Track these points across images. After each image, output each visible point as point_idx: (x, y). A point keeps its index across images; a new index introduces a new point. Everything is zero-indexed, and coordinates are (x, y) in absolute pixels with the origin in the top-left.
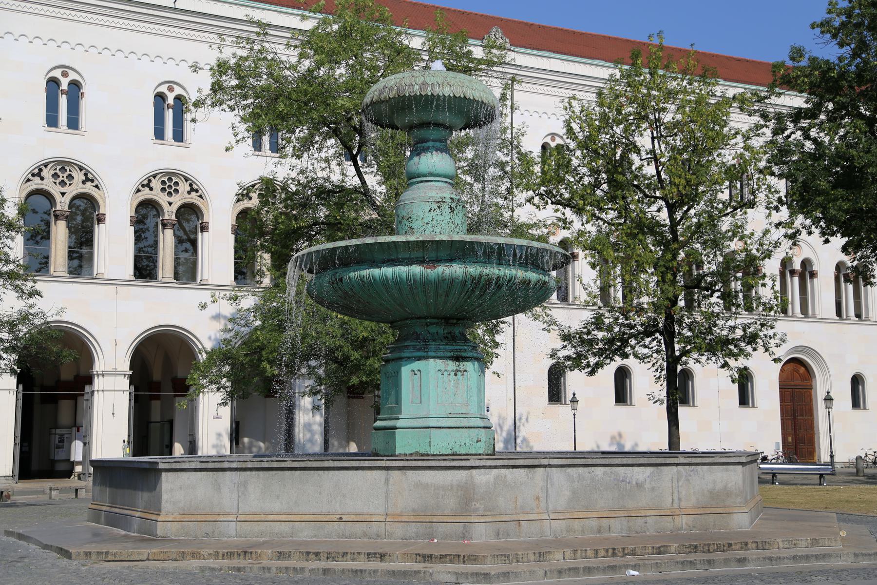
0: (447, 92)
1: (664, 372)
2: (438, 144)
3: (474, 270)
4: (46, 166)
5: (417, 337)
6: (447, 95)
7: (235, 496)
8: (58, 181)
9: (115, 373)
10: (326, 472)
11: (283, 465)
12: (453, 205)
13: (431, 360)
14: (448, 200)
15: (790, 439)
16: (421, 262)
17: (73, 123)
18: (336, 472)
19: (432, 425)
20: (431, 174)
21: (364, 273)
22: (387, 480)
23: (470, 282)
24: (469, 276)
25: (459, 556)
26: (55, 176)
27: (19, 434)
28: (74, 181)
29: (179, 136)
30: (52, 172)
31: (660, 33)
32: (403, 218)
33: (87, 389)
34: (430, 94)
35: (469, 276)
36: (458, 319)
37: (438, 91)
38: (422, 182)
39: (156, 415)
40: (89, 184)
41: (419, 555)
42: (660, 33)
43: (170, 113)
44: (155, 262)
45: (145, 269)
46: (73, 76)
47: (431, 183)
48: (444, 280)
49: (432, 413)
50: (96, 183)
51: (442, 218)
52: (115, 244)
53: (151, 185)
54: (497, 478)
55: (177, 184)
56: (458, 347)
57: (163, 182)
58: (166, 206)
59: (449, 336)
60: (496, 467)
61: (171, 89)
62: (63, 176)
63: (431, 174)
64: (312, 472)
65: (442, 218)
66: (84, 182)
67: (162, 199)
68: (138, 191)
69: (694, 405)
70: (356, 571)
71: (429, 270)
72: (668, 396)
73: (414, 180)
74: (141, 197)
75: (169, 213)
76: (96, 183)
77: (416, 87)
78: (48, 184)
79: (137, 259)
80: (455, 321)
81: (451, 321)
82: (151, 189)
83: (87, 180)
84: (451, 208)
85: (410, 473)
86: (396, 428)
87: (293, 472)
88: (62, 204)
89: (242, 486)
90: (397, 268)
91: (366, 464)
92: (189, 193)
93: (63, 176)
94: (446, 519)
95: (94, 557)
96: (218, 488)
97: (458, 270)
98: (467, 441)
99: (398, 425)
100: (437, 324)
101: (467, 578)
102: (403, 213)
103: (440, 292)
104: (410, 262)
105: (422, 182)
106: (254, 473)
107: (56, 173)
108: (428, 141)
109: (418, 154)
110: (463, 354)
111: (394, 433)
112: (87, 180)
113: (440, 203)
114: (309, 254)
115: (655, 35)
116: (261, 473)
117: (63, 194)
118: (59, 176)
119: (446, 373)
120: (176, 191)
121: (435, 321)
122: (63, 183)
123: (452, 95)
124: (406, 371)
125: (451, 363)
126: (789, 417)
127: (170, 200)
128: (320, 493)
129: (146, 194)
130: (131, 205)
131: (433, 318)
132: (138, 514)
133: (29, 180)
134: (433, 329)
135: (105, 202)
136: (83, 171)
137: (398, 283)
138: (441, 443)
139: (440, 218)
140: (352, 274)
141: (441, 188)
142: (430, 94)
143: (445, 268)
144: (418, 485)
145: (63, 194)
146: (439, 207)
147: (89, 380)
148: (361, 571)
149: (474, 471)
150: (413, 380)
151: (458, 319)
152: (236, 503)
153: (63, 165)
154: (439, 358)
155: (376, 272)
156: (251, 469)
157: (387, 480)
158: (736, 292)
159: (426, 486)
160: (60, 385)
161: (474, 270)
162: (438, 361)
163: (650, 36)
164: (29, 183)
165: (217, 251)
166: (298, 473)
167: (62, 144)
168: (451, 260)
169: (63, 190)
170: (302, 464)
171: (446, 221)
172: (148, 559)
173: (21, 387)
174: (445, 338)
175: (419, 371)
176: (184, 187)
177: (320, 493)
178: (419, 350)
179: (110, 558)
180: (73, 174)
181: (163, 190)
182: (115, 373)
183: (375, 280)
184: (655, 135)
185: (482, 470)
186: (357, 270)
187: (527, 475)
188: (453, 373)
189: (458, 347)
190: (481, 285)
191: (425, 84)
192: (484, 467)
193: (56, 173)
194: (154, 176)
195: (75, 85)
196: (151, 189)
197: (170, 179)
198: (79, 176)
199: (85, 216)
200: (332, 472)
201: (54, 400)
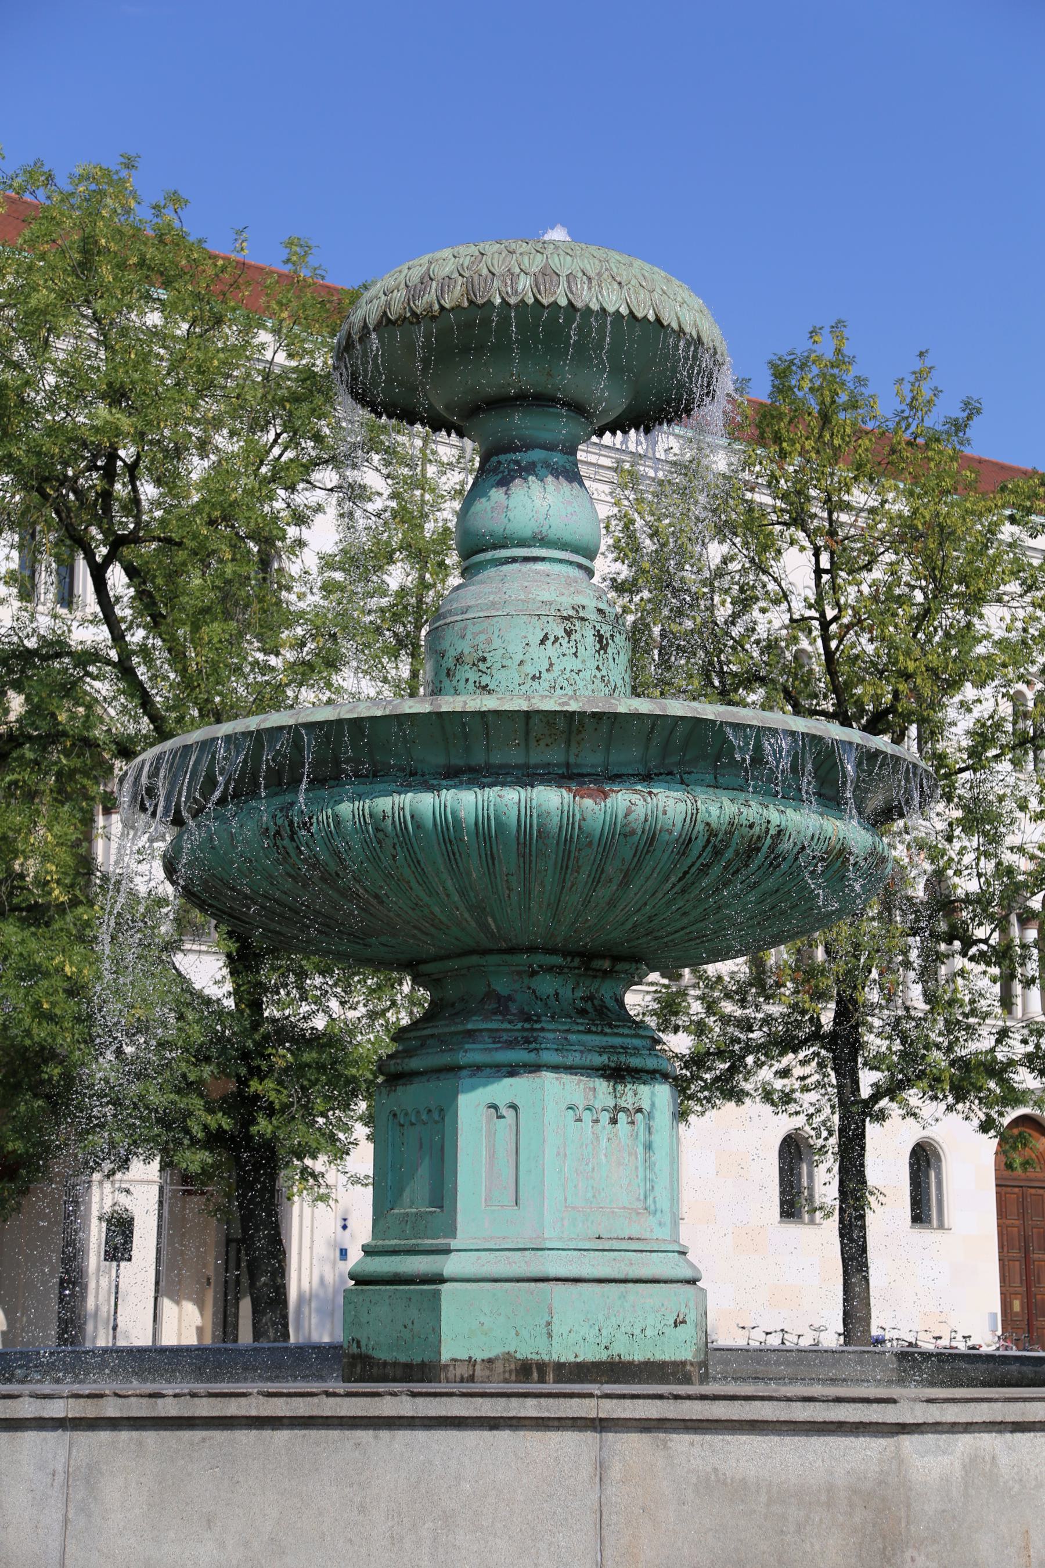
0: (613, 301)
1: (834, 1140)
2: (556, 458)
3: (718, 808)
5: (501, 1005)
6: (611, 309)
7: (53, 1517)
10: (385, 1435)
11: (233, 1408)
12: (606, 630)
13: (548, 1076)
14: (593, 616)
15: (1017, 1306)
16: (566, 776)
18: (421, 1436)
19: (553, 1271)
20: (543, 541)
21: (384, 804)
22: (601, 1468)
23: (701, 842)
24: (700, 827)
31: (837, 326)
32: (459, 660)
34: (563, 302)
35: (700, 827)
36: (616, 959)
37: (586, 297)
38: (514, 560)
42: (837, 326)
47: (539, 566)
48: (627, 834)
49: (551, 1236)
51: (577, 664)
54: (972, 1463)
56: (617, 1041)
59: (589, 1007)
60: (968, 1427)
63: (543, 541)
64: (335, 1434)
69: (941, 1226)
71: (588, 802)
72: (843, 1201)
73: (481, 557)
77: (524, 283)
80: (606, 965)
81: (597, 964)
84: (600, 637)
85: (681, 1441)
86: (441, 1280)
87: (267, 1434)
89: (79, 1485)
90: (449, 796)
91: (530, 1408)
97: (668, 805)
98: (650, 1321)
102: (465, 647)
103: (610, 870)
104: (528, 776)
105: (514, 560)
106: (124, 1435)
108: (528, 446)
109: (504, 483)
110: (635, 1062)
111: (437, 1295)
113: (571, 620)
114: (207, 745)
115: (827, 329)
116: (150, 1437)
119: (587, 1116)
121: (558, 960)
123: (624, 311)
124: (471, 1106)
125: (602, 1086)
126: (1015, 1253)
128: (362, 1509)
131: (553, 951)
134: (547, 985)
137: (488, 834)
138: (578, 1330)
139: (570, 663)
140: (345, 809)
141: (569, 582)
142: (563, 302)
143: (635, 798)
144: (711, 1484)
146: (569, 633)
149: (907, 1441)
150: (491, 1134)
151: (616, 959)
152: (54, 1545)
154: (570, 1069)
155: (423, 803)
156: (114, 1424)
157: (601, 1468)
158: (1024, 946)
159: (738, 1490)
161: (718, 808)
162: (567, 1078)
163: (813, 332)
166: (282, 1436)
168: (647, 778)
170: (301, 1407)
171: (587, 675)
174: (582, 1012)
175: (514, 1107)
177: (362, 1509)
178: (511, 1045)
183: (418, 826)
184: (825, 562)
185: (930, 1438)
186: (360, 797)
188: (605, 1117)
189: (617, 1041)
190: (729, 854)
191: (547, 274)
192: (936, 1428)
200: (403, 1436)
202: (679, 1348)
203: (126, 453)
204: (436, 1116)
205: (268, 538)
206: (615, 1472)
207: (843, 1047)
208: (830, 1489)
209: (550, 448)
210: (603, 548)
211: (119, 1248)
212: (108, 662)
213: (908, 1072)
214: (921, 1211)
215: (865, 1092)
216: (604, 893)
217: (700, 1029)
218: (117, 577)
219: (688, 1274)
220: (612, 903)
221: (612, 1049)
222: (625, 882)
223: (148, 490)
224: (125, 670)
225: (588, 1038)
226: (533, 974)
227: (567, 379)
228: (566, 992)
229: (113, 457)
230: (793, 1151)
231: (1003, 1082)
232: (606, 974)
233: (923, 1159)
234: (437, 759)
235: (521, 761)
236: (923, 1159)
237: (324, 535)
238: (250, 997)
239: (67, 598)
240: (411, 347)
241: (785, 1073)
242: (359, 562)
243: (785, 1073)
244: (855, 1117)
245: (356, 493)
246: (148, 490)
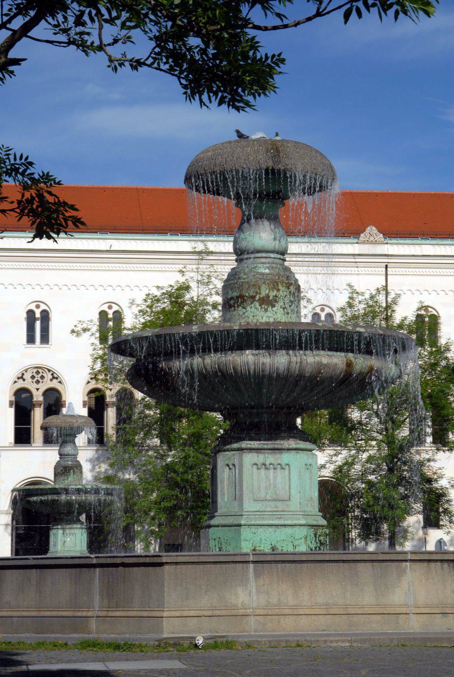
4: (26, 371)
8: (41, 381)
17: (45, 339)
28: (45, 380)
30: (31, 375)
40: (55, 380)
46: (43, 307)
50: (59, 380)
53: (24, 377)
58: (34, 392)
61: (322, 310)
66: (51, 380)
67: (32, 387)
68: (15, 382)
76: (59, 380)
78: (29, 384)
88: (38, 397)
93: (38, 377)
99: (242, 522)
107: (33, 376)
118: (35, 377)
122: (38, 382)
129: (21, 384)
130: (83, 392)
133: (15, 382)
135: (65, 392)
136: (51, 372)
145: (38, 389)
153: (38, 369)
160: (334, 421)
164: (16, 384)
167: (38, 355)
173: (14, 523)
180: (45, 375)
193: (33, 376)
197: (38, 373)
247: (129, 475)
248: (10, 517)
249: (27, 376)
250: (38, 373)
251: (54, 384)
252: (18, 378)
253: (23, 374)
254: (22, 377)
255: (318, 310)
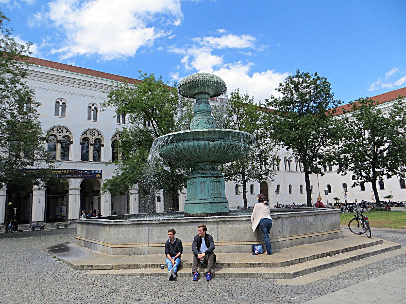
4: (55, 127)
9: (75, 189)
25: (267, 263)
26: (58, 130)
27: (46, 207)
29: (95, 119)
33: (67, 194)
39: (191, 215)
40: (68, 133)
41: (248, 263)
43: (92, 110)
44: (88, 156)
45: (85, 158)
46: (63, 101)
51: (209, 126)
52: (75, 151)
55: (94, 133)
56: (217, 173)
57: (90, 132)
61: (93, 105)
62: (60, 130)
65: (209, 126)
67: (90, 137)
68: (83, 135)
70: (222, 274)
74: (84, 136)
75: (92, 141)
79: (82, 154)
82: (87, 134)
83: (67, 131)
92: (98, 135)
93: (60, 130)
94: (246, 243)
95: (86, 268)
96: (139, 232)
100: (209, 164)
101: (279, 276)
110: (219, 175)
112: (67, 131)
117: (60, 136)
120: (94, 135)
121: (209, 163)
122: (60, 132)
127: (93, 137)
129: (85, 135)
132: (101, 243)
134: (207, 166)
145: (60, 136)
147: (68, 191)
148: (224, 274)
151: (216, 162)
159: (235, 229)
165: (106, 153)
169: (60, 134)
172: (112, 269)
173: (47, 194)
174: (212, 169)
176: (97, 134)
179: (94, 268)
181: (90, 134)
182: (75, 189)
187: (276, 222)
188: (216, 182)
189: (217, 173)
190: (230, 148)
194: (88, 130)
195: (64, 103)
196: (87, 134)
197: (92, 131)
198: (65, 130)
199: (98, 144)
201: (57, 198)
202: (226, 211)
203: (155, 107)
204: (265, 230)
205: (172, 116)
206: (219, 228)
207: (243, 174)
208: (247, 228)
209: (205, 99)
210: (203, 252)
211: (159, 201)
212: (153, 132)
213: (250, 176)
214: (252, 193)
215: (246, 179)
216: (214, 154)
217: (225, 172)
218: (154, 122)
219: (226, 201)
220: (215, 155)
221: (216, 174)
222: (217, 153)
223: (158, 112)
224: (156, 132)
225: (213, 173)
226: (206, 165)
227: (206, 90)
228: (210, 167)
229: (153, 108)
230: (237, 186)
231: (261, 177)
232: (215, 164)
233: (252, 186)
234: (192, 138)
235: (203, 137)
236: (252, 186)
237: (179, 115)
238: (172, 171)
239: (149, 125)
240: (187, 87)
241: (236, 177)
242: (183, 118)
243: (236, 177)
244: (245, 181)
245: (182, 111)
246: (158, 112)
247: (183, 146)
248: (45, 192)
249: (88, 132)
250: (60, 128)
251: (101, 138)
252: (114, 136)
253: (100, 135)
254: (86, 133)
255: (91, 105)
